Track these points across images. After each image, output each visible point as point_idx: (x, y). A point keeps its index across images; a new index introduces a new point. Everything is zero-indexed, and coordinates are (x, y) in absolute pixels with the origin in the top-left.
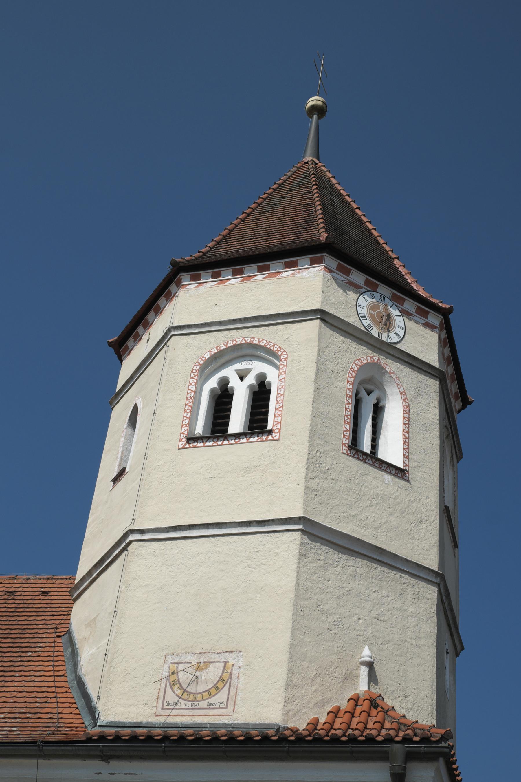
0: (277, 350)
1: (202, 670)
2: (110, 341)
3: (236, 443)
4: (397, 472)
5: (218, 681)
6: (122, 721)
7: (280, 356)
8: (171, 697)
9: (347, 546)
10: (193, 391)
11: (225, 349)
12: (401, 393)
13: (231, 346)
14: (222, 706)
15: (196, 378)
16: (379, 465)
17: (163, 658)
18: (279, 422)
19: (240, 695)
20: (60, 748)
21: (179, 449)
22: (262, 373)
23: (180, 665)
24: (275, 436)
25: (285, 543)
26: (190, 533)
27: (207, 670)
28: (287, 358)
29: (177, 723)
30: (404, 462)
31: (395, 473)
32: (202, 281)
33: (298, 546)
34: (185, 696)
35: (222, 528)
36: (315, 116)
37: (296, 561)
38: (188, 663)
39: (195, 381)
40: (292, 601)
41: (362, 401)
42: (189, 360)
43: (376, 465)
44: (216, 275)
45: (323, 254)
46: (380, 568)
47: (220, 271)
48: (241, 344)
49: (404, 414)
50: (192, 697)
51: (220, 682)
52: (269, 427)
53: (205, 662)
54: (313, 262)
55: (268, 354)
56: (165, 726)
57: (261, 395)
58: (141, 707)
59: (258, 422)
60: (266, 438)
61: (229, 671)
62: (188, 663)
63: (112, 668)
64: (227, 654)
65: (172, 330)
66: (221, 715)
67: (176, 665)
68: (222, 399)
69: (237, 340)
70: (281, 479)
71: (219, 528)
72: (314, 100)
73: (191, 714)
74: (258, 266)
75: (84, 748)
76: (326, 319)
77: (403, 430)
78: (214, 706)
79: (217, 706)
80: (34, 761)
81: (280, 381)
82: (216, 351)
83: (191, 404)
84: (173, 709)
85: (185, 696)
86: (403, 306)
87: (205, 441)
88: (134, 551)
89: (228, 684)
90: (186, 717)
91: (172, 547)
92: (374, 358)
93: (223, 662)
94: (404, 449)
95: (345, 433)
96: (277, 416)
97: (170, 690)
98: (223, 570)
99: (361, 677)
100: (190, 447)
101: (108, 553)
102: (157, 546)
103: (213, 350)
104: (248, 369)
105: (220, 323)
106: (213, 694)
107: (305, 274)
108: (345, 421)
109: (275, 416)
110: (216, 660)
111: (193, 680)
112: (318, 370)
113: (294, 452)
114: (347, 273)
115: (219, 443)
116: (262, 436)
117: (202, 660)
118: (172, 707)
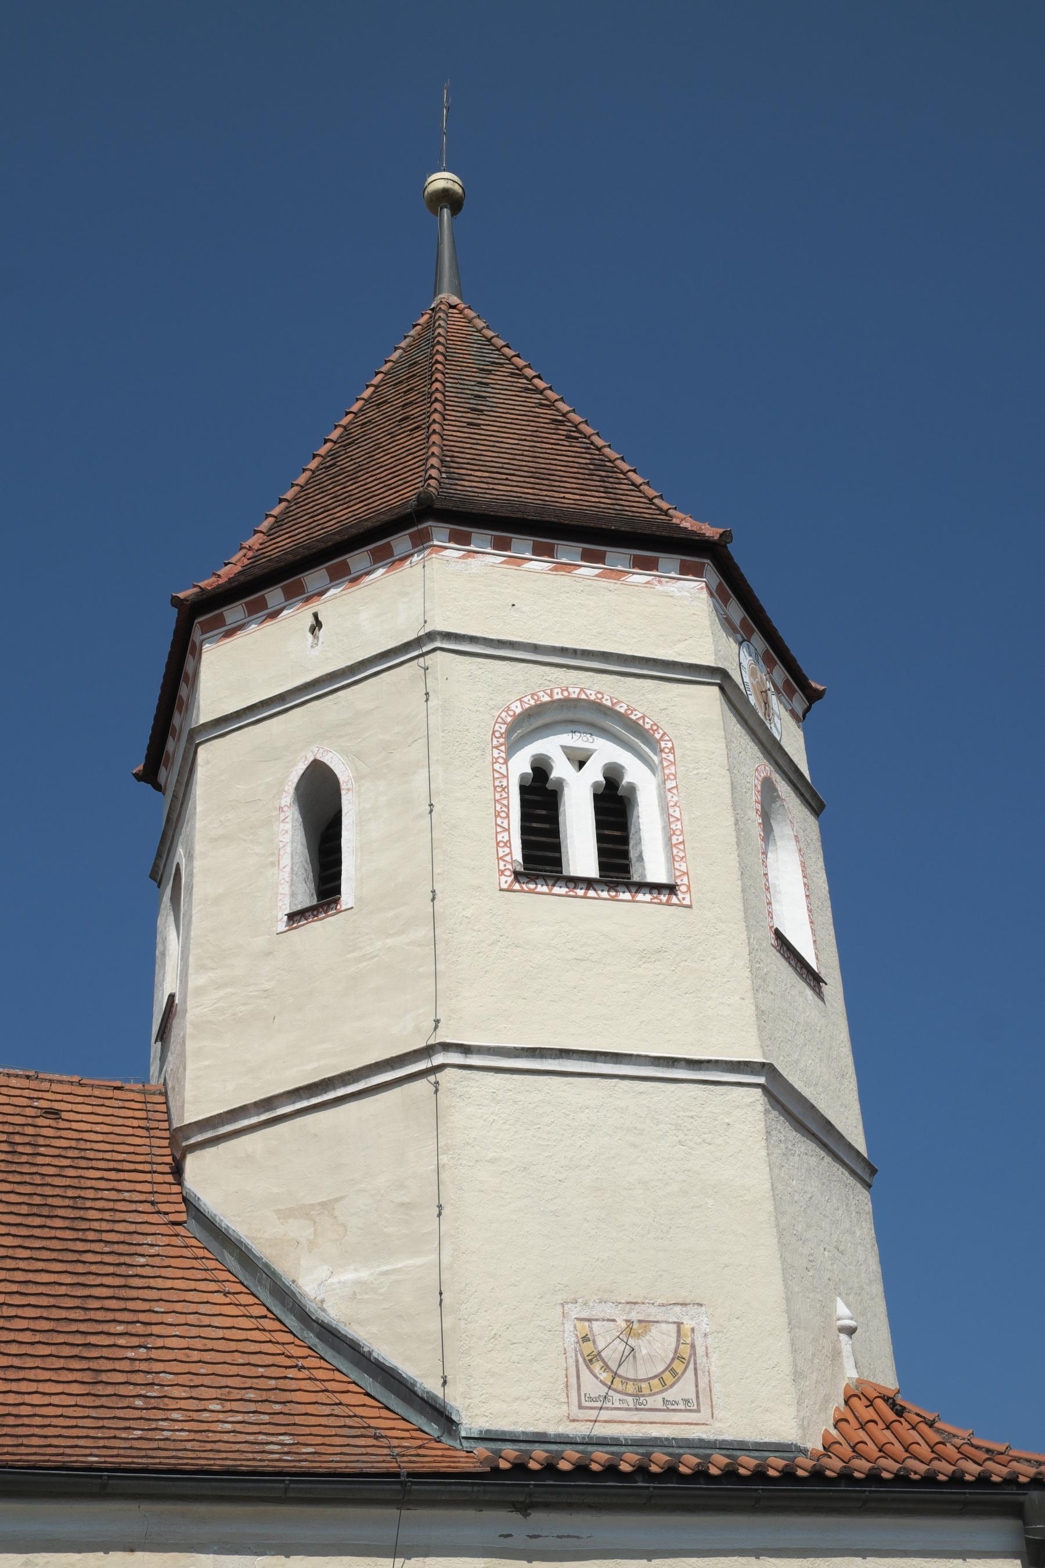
0: (652, 729)
1: (638, 1336)
2: (182, 595)
3: (613, 899)
5: (673, 1359)
6: (506, 1429)
7: (658, 741)
8: (592, 1386)
9: (801, 1117)
13: (560, 700)
14: (691, 1406)
17: (559, 1309)
19: (717, 1388)
20: (448, 1488)
21: (501, 890)
23: (595, 1324)
24: (684, 899)
26: (560, 1065)
27: (648, 1337)
28: (673, 748)
29: (616, 1435)
32: (472, 548)
33: (762, 1116)
34: (617, 1384)
35: (621, 1063)
36: (446, 213)
37: (764, 1143)
38: (609, 1320)
40: (773, 1219)
42: (481, 709)
44: (501, 545)
45: (705, 561)
46: (828, 1159)
48: (578, 700)
50: (631, 1388)
51: (676, 1361)
53: (640, 1321)
54: (685, 570)
55: (634, 733)
56: (595, 1441)
57: (613, 805)
58: (539, 1402)
59: (616, 864)
61: (689, 1341)
62: (609, 1320)
63: (463, 1322)
64: (677, 1309)
65: (438, 638)
66: (691, 1424)
67: (587, 1324)
68: (540, 797)
71: (616, 1063)
72: (441, 180)
73: (635, 1419)
74: (584, 549)
75: (497, 1489)
78: (675, 1407)
79: (681, 1406)
80: (392, 1512)
84: (601, 1408)
85: (617, 1384)
89: (691, 1366)
90: (628, 1425)
91: (528, 1088)
93: (675, 1323)
97: (588, 1372)
98: (635, 1146)
99: (844, 1354)
100: (522, 891)
101: (349, 1074)
103: (647, 720)
104: (588, 750)
105: (536, 648)
106: (668, 1383)
110: (659, 1318)
111: (626, 1354)
112: (733, 788)
113: (723, 936)
114: (725, 601)
116: (659, 893)
117: (634, 1316)
118: (599, 1404)
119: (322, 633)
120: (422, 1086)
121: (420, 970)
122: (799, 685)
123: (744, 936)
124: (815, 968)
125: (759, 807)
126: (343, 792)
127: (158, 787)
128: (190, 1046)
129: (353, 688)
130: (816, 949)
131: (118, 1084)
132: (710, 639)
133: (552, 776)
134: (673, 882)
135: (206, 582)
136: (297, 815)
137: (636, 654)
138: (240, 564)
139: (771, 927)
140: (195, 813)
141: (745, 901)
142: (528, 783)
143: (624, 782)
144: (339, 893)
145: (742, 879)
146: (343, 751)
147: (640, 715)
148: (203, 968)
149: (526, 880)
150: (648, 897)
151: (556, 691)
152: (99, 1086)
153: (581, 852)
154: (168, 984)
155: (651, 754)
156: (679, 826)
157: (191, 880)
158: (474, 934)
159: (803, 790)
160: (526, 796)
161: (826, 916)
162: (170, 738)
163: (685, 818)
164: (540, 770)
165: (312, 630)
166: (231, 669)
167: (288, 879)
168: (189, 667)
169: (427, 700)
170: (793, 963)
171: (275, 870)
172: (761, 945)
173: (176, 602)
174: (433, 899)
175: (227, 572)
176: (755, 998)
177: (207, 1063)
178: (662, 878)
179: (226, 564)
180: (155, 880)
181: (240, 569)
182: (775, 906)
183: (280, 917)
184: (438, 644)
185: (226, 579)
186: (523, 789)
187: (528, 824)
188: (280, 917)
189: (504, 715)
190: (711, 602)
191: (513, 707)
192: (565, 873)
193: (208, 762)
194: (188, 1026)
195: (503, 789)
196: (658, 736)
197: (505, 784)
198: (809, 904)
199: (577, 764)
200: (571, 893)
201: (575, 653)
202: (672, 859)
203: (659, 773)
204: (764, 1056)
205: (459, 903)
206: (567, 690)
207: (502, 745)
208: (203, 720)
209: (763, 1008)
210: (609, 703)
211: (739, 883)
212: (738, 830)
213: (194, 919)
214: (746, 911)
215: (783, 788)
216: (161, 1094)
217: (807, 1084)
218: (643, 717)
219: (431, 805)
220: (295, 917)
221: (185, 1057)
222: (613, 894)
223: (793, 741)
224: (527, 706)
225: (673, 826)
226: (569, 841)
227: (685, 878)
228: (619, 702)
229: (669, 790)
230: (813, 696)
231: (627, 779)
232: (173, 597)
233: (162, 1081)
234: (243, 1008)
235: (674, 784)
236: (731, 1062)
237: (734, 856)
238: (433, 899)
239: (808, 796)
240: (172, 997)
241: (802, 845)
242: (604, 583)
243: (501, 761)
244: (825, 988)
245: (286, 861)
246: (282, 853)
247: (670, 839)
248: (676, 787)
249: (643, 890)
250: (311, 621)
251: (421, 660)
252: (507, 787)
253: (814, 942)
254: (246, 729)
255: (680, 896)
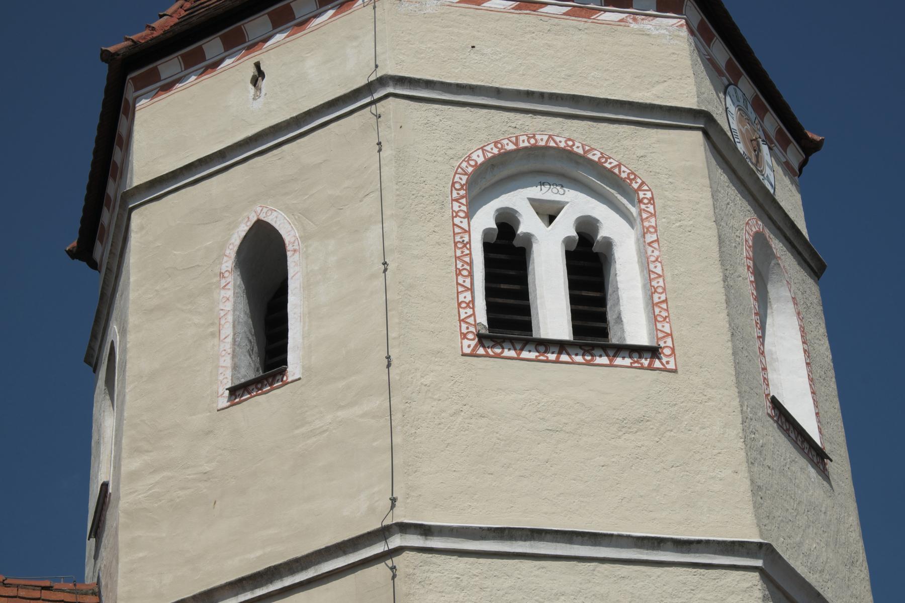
0: (628, 178)
2: (112, 49)
3: (588, 364)
7: (636, 191)
13: (526, 148)
21: (464, 355)
22: (589, 216)
24: (668, 362)
25: (733, 593)
26: (532, 546)
28: (652, 198)
42: (439, 159)
48: (546, 148)
57: (588, 263)
59: (592, 325)
65: (391, 83)
68: (507, 256)
70: (697, 457)
76: (711, 132)
88: (411, 571)
91: (496, 573)
100: (487, 356)
102: (462, 565)
103: (623, 168)
105: (498, 93)
112: (721, 241)
113: (711, 403)
114: (708, 40)
115: (552, 357)
116: (640, 357)
119: (264, 84)
120: (380, 571)
121: (375, 444)
122: (793, 135)
123: (736, 403)
124: (816, 438)
125: (751, 263)
126: (289, 254)
127: (94, 265)
128: (123, 537)
129: (298, 141)
130: (819, 422)
131: (47, 583)
132: (692, 80)
133: (519, 232)
134: (655, 344)
135: (139, 35)
136: (239, 281)
137: (609, 97)
138: (176, 16)
139: (767, 395)
140: (129, 283)
141: (737, 364)
142: (493, 239)
143: (599, 237)
144: (286, 364)
145: (732, 341)
146: (289, 210)
147: (615, 163)
148: (138, 451)
149: (492, 344)
150: (627, 361)
151: (521, 138)
152: (25, 586)
153: (553, 313)
154: (102, 472)
155: (629, 206)
156: (661, 284)
157: (125, 357)
158: (435, 403)
159: (800, 249)
160: (492, 255)
161: (831, 387)
162: (105, 209)
163: (668, 275)
164: (506, 225)
165: (255, 82)
166: (165, 128)
167: (230, 351)
168: (122, 129)
169: (380, 151)
170: (793, 435)
171: (216, 341)
172: (756, 413)
173: (106, 57)
174: (389, 366)
175: (162, 25)
176: (750, 471)
177: (141, 555)
178: (643, 339)
179: (161, 16)
180: (90, 364)
181: (177, 21)
182: (771, 376)
183: (221, 392)
184: (390, 90)
185: (162, 32)
186: (488, 247)
187: (494, 286)
188: (221, 392)
189: (464, 165)
190: (691, 40)
191: (474, 156)
192: (535, 335)
193: (142, 228)
194: (121, 514)
195: (465, 246)
196: (635, 186)
197: (466, 239)
198: (810, 373)
199: (547, 219)
200: (542, 358)
201: (542, 97)
202: (654, 319)
203: (638, 226)
204: (761, 536)
205: (417, 369)
206: (534, 137)
207: (462, 197)
208: (136, 182)
209: (759, 484)
210: (580, 151)
211: (730, 344)
212: (728, 288)
213: (128, 398)
214: (737, 374)
215: (778, 246)
216: (94, 594)
217: (811, 570)
218: (619, 166)
219: (385, 263)
220: (236, 392)
221: (118, 550)
222: (589, 358)
223: (790, 200)
224: (490, 155)
225: (654, 283)
226: (539, 301)
227: (669, 340)
228: (592, 149)
229: (649, 244)
230: (809, 148)
231: (603, 233)
232: (103, 52)
233: (95, 580)
234: (181, 493)
235: (654, 237)
236: (724, 542)
237: (723, 315)
238: (389, 366)
239: (806, 256)
240: (105, 486)
241: (801, 308)
242: (573, 22)
243: (462, 214)
244: (830, 466)
245: (227, 330)
246: (223, 322)
247: (652, 297)
248: (657, 241)
249: (622, 354)
250: (252, 71)
251: (373, 107)
252: (469, 242)
253: (817, 414)
254: (183, 191)
255: (664, 360)
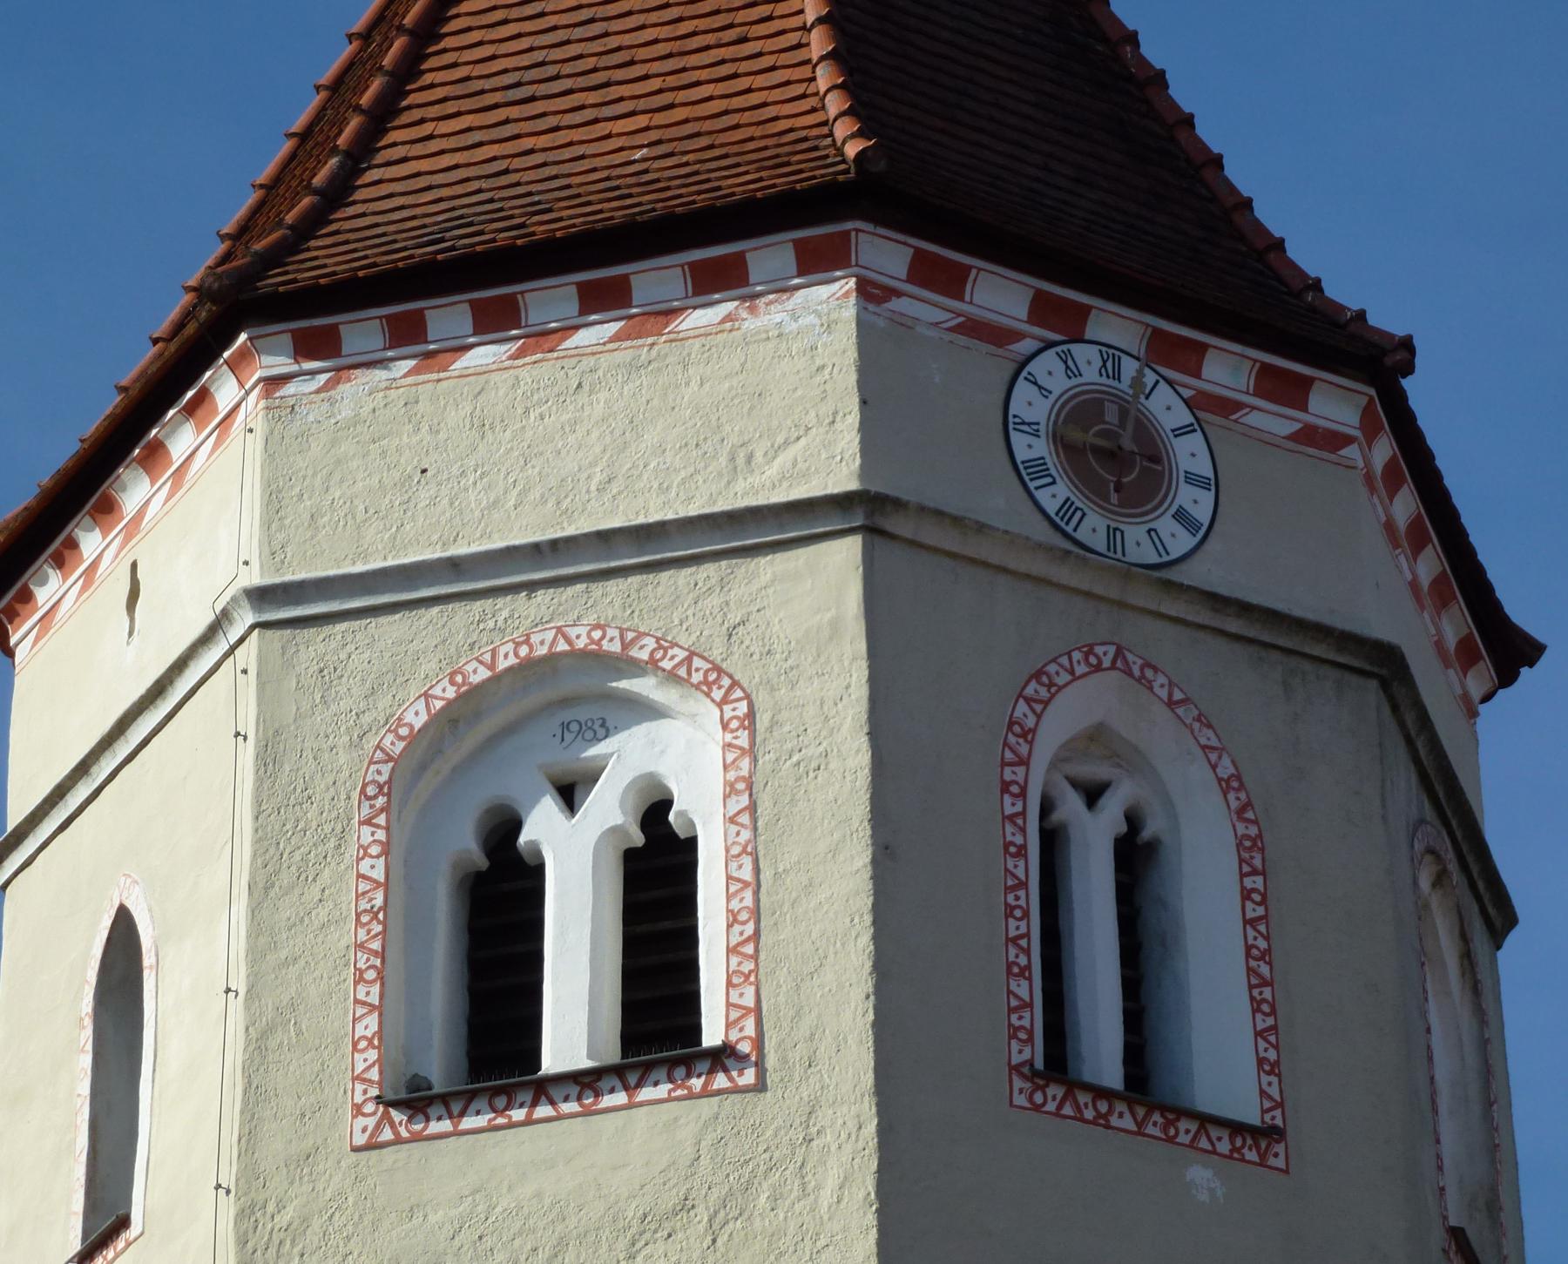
3: (588, 1113)
4: (1239, 1143)
10: (377, 884)
11: (489, 679)
12: (1225, 785)
13: (510, 669)
15: (381, 820)
16: (1165, 1130)
18: (748, 1010)
21: (355, 1149)
30: (1263, 1093)
31: (1234, 1149)
39: (381, 835)
41: (1067, 839)
43: (1150, 1130)
45: (849, 225)
47: (421, 311)
48: (552, 658)
49: (1242, 875)
52: (711, 1037)
57: (657, 870)
59: (658, 1018)
60: (705, 1085)
69: (535, 639)
77: (1248, 948)
81: (732, 820)
82: (451, 693)
83: (376, 945)
86: (1198, 376)
87: (456, 1108)
92: (1099, 650)
94: (1258, 1034)
95: (1014, 1017)
96: (735, 980)
107: (774, 314)
108: (1009, 965)
109: (729, 984)
114: (951, 282)
115: (518, 1114)
116: (689, 1075)
200: (501, 1121)
206: (527, 642)
242: (640, 349)
